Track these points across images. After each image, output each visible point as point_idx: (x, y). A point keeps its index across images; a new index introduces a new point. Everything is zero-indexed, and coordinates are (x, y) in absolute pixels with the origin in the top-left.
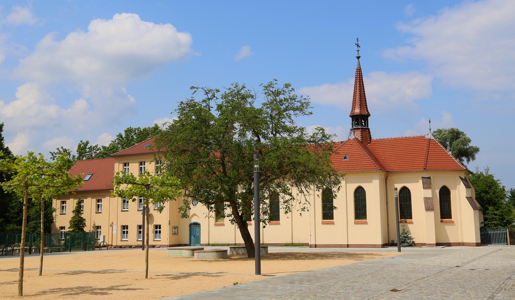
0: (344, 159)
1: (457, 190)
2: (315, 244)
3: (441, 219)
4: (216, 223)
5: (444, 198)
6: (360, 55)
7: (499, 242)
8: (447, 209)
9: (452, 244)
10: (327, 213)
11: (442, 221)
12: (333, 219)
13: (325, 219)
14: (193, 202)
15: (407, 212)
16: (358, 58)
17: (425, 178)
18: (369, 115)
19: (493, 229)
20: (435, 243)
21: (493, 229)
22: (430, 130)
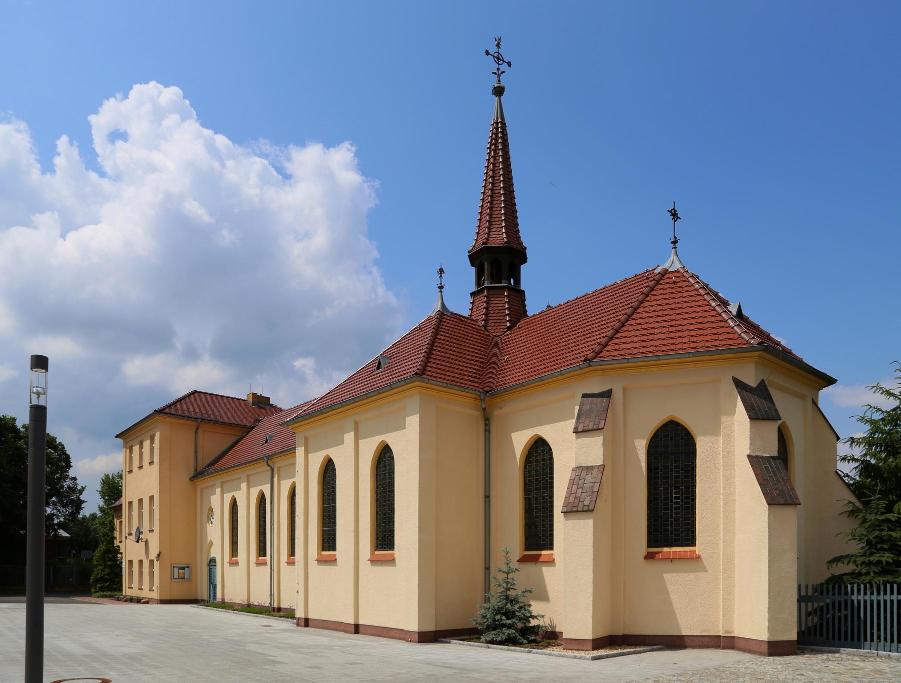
1: (721, 439)
3: (649, 546)
4: (233, 559)
7: (892, 641)
8: (677, 508)
9: (688, 642)
11: (649, 557)
15: (544, 526)
19: (870, 583)
20: (310, 617)
21: (871, 587)
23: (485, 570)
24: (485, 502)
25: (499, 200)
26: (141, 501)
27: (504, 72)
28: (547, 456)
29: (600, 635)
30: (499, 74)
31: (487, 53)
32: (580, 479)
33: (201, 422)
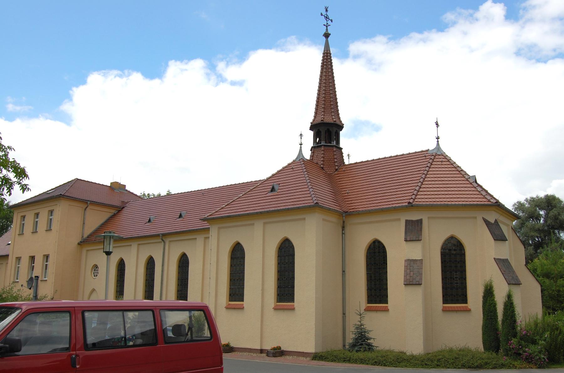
2: (259, 348)
3: (444, 303)
6: (329, 32)
14: (95, 272)
23: (343, 315)
24: (343, 274)
25: (329, 96)
26: (33, 258)
27: (330, 25)
28: (381, 251)
29: (319, 350)
30: (327, 26)
31: (322, 15)
32: (410, 267)
33: (90, 203)
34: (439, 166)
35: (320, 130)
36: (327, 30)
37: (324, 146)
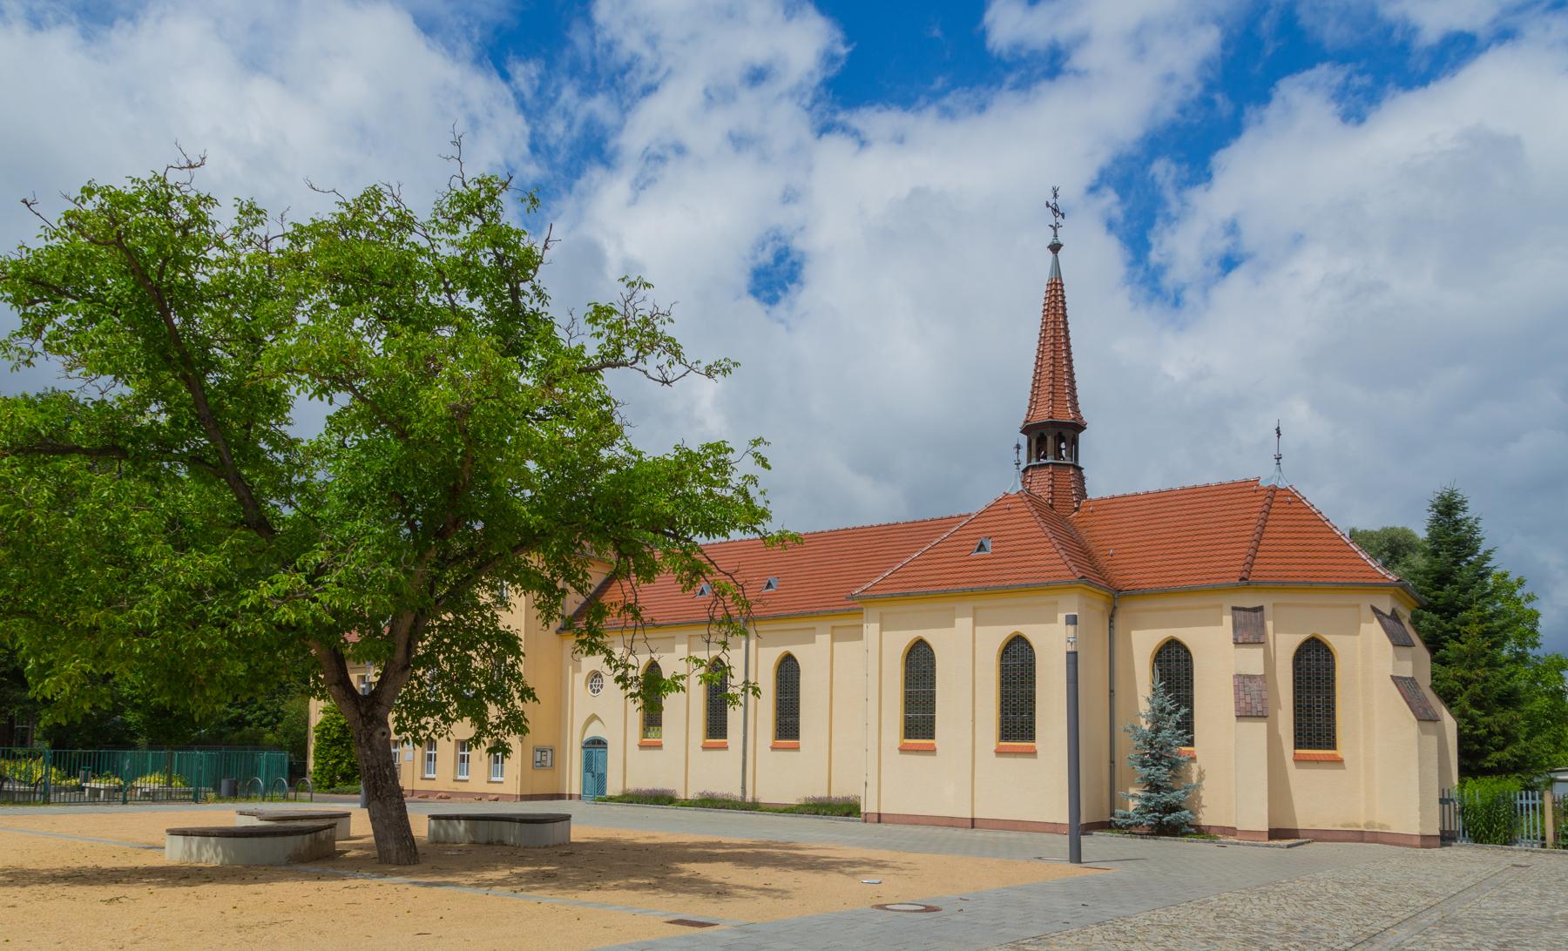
0: (979, 550)
2: (970, 816)
5: (1309, 678)
6: (1061, 240)
10: (917, 717)
12: (931, 736)
13: (910, 738)
16: (1055, 248)
17: (1244, 609)
18: (1078, 427)
20: (1266, 829)
22: (1278, 459)
31: (1048, 205)
34: (1285, 511)
35: (1064, 434)
36: (1056, 236)
37: (1054, 464)
